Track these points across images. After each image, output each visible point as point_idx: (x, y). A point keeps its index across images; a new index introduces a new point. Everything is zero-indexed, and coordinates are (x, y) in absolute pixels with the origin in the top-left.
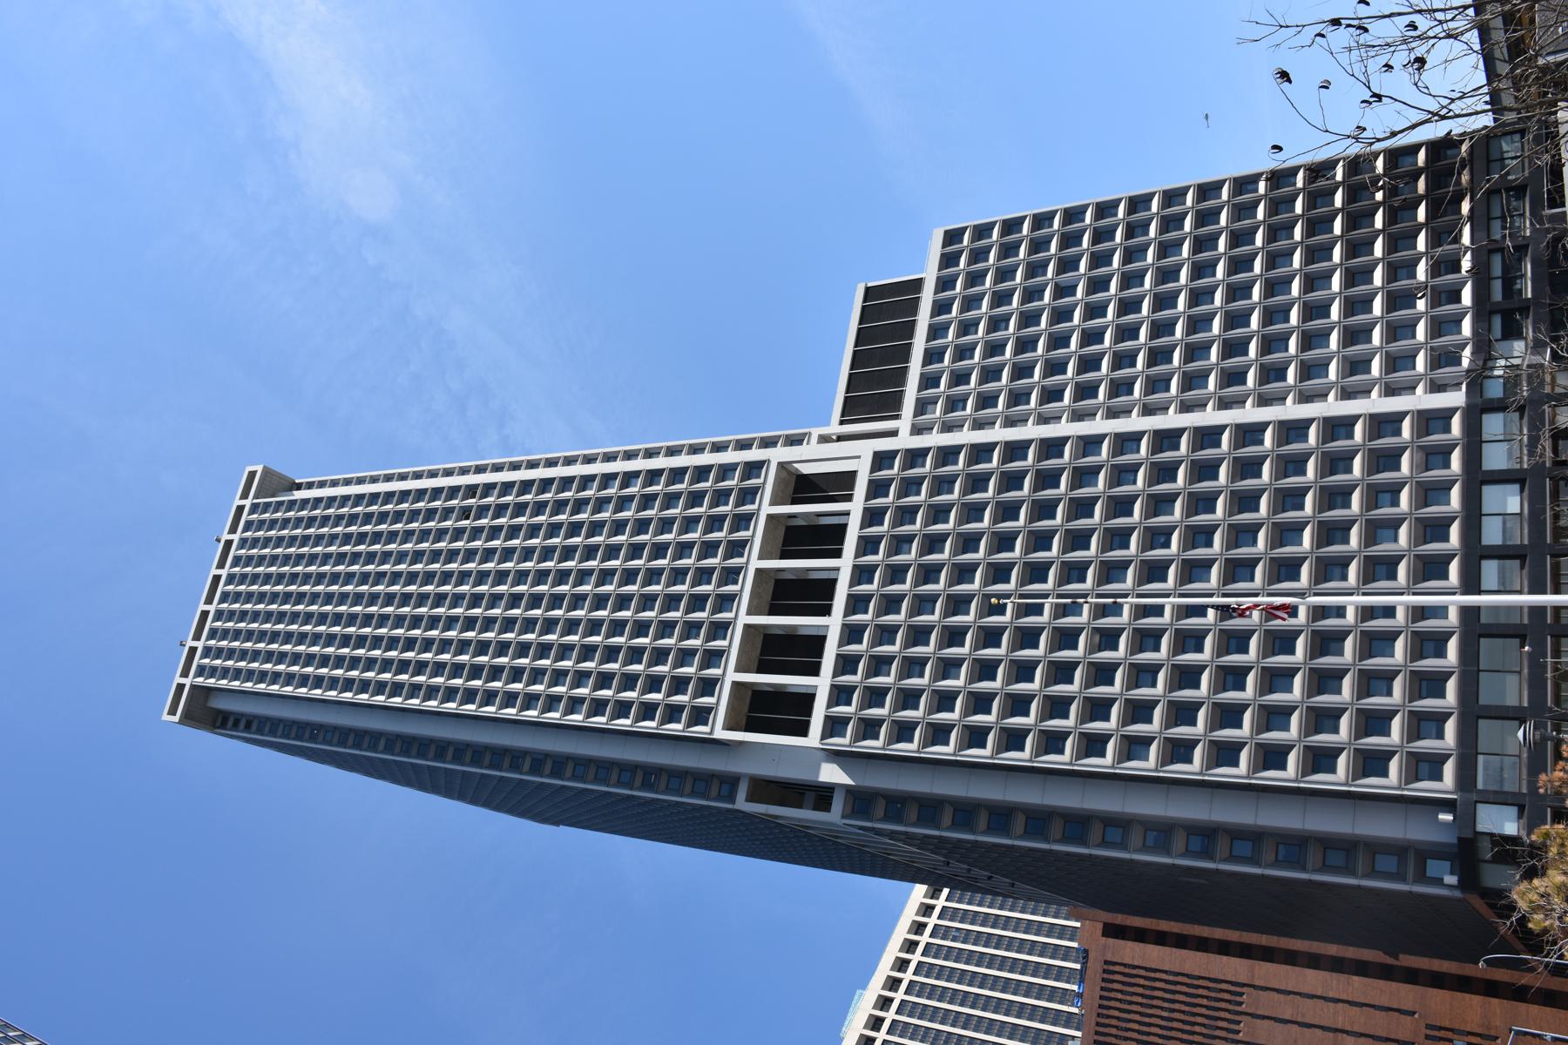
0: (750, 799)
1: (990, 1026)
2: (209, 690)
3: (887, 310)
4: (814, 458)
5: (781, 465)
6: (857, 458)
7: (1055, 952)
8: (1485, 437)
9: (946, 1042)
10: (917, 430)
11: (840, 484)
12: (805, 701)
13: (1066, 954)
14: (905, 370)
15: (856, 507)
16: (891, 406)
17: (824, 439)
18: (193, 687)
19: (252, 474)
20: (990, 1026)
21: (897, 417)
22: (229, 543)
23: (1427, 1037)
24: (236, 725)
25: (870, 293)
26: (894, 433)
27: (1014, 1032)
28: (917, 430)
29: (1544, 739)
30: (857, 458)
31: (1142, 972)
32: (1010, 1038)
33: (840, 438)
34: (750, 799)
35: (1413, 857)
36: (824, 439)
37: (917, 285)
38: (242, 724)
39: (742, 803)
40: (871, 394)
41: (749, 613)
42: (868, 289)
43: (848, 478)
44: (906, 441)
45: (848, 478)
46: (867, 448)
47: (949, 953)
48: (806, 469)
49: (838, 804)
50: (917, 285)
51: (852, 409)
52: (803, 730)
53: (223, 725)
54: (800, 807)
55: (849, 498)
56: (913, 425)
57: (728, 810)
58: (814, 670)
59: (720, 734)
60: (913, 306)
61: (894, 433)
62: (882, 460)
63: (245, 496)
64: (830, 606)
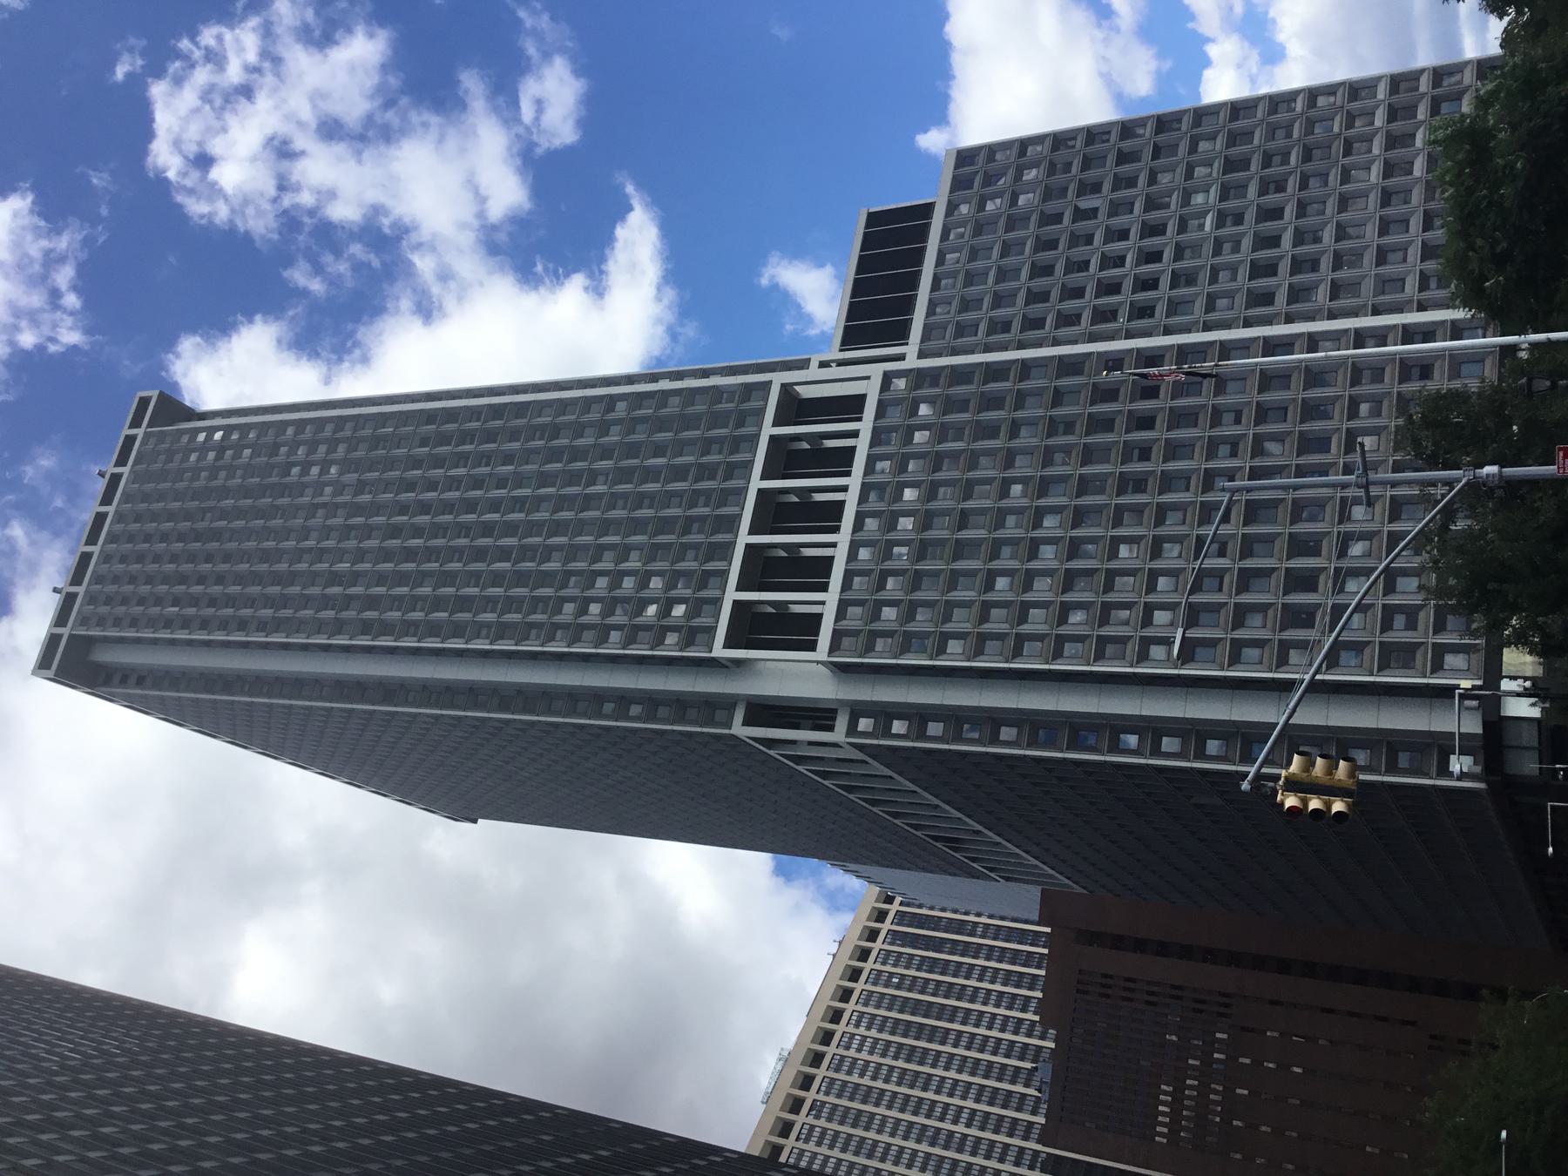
0: (746, 723)
2: (90, 642)
4: (815, 385)
6: (867, 381)
9: (849, 1173)
10: (922, 355)
11: (852, 407)
13: (1028, 960)
14: (923, 249)
15: (865, 426)
16: (899, 334)
17: (823, 365)
18: (71, 636)
19: (144, 402)
21: (860, 419)
22: (116, 479)
23: (1430, 1047)
24: (124, 681)
25: (873, 219)
26: (901, 357)
28: (922, 355)
30: (867, 381)
33: (841, 363)
34: (746, 723)
36: (823, 365)
37: (928, 209)
38: (133, 681)
39: (739, 729)
42: (870, 215)
43: (860, 400)
44: (912, 362)
45: (860, 400)
46: (877, 371)
48: (806, 392)
49: (842, 723)
50: (928, 209)
52: (812, 646)
53: (107, 682)
55: (848, 474)
57: (718, 737)
59: (719, 651)
60: (922, 234)
61: (901, 357)
62: (887, 378)
63: (136, 423)
64: (816, 642)
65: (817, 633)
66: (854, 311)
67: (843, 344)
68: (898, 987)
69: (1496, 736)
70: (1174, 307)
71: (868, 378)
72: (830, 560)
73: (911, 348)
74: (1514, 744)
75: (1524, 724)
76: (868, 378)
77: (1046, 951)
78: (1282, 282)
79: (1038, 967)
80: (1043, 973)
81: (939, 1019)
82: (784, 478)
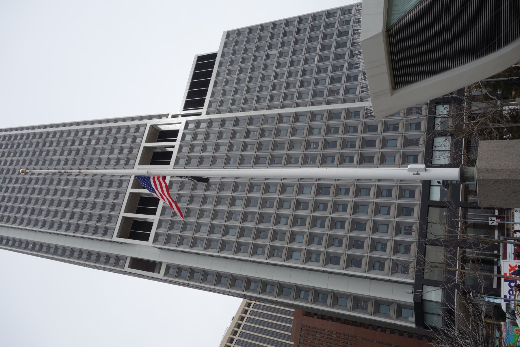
1: (262, 340)
3: (204, 65)
5: (153, 127)
7: (283, 320)
8: (429, 220)
9: (250, 346)
11: (172, 135)
12: (149, 225)
15: (177, 144)
20: (262, 340)
26: (200, 114)
27: (270, 342)
28: (208, 113)
29: (511, 130)
31: (438, 265)
32: (268, 344)
33: (183, 116)
35: (400, 307)
40: (195, 98)
41: (132, 188)
44: (204, 117)
47: (260, 314)
51: (188, 105)
54: (153, 271)
56: (405, 253)
58: (154, 212)
59: (115, 239)
60: (212, 65)
61: (200, 114)
62: (187, 123)
65: (150, 230)
66: (190, 95)
67: (184, 108)
68: (262, 310)
69: (420, 307)
70: (332, 92)
71: (180, 123)
72: (151, 224)
73: (204, 110)
74: (429, 312)
75: (434, 304)
76: (180, 123)
77: (293, 318)
78: (341, 86)
79: (290, 324)
80: (291, 326)
81: (278, 321)
82: (158, 141)
